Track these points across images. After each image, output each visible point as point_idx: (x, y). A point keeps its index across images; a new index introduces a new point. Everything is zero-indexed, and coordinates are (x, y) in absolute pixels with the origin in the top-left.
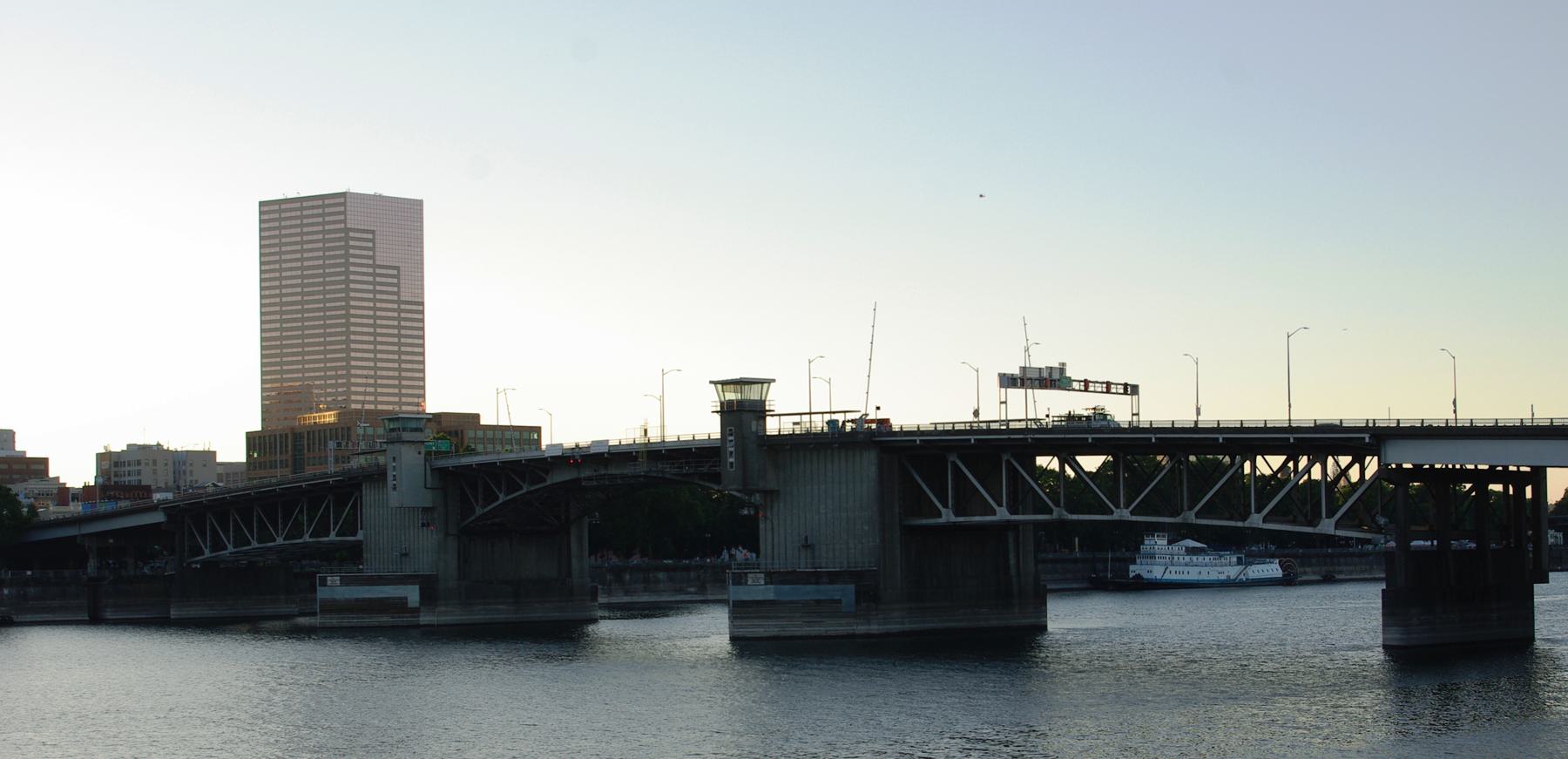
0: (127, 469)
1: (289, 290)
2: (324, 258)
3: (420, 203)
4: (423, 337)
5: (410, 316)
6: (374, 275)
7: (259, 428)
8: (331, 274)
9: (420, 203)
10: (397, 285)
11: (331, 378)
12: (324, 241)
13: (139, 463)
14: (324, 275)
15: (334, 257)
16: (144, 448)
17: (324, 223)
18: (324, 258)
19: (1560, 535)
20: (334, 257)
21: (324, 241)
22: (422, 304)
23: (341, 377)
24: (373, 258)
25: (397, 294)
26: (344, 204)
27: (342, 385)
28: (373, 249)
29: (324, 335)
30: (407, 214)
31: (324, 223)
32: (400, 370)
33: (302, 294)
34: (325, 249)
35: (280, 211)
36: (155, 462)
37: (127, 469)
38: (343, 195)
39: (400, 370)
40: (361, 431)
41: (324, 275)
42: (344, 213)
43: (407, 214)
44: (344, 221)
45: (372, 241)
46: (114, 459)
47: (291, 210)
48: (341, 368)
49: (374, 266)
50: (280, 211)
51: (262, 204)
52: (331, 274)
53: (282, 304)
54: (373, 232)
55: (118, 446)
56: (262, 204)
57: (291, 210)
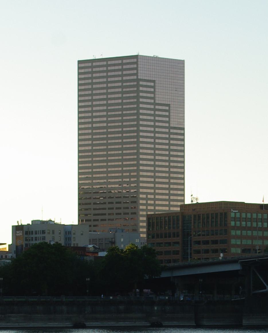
0: (34, 236)
1: (98, 119)
2: (122, 98)
3: (182, 62)
4: (183, 151)
5: (175, 137)
6: (155, 110)
7: (64, 211)
8: (127, 109)
9: (182, 62)
10: (169, 117)
11: (126, 177)
12: (122, 87)
13: (43, 232)
14: (122, 110)
15: (129, 98)
16: (43, 222)
17: (122, 76)
18: (122, 98)
19: (221, 259)
20: (129, 98)
21: (122, 87)
22: (183, 129)
23: (134, 177)
24: (154, 98)
25: (169, 122)
26: (136, 63)
27: (134, 182)
28: (154, 93)
29: (122, 149)
30: (176, 68)
31: (122, 76)
32: (169, 172)
33: (107, 122)
34: (123, 93)
35: (107, 66)
36: (53, 232)
37: (34, 236)
38: (136, 57)
39: (169, 172)
40: (233, 215)
41: (122, 110)
42: (136, 69)
43: (176, 68)
44: (136, 74)
45: (154, 87)
46: (25, 229)
47: (114, 65)
48: (134, 171)
49: (155, 104)
50: (122, 64)
51: (80, 62)
52: (127, 109)
53: (93, 128)
54: (154, 81)
55: (26, 221)
56: (80, 62)
57: (114, 65)
